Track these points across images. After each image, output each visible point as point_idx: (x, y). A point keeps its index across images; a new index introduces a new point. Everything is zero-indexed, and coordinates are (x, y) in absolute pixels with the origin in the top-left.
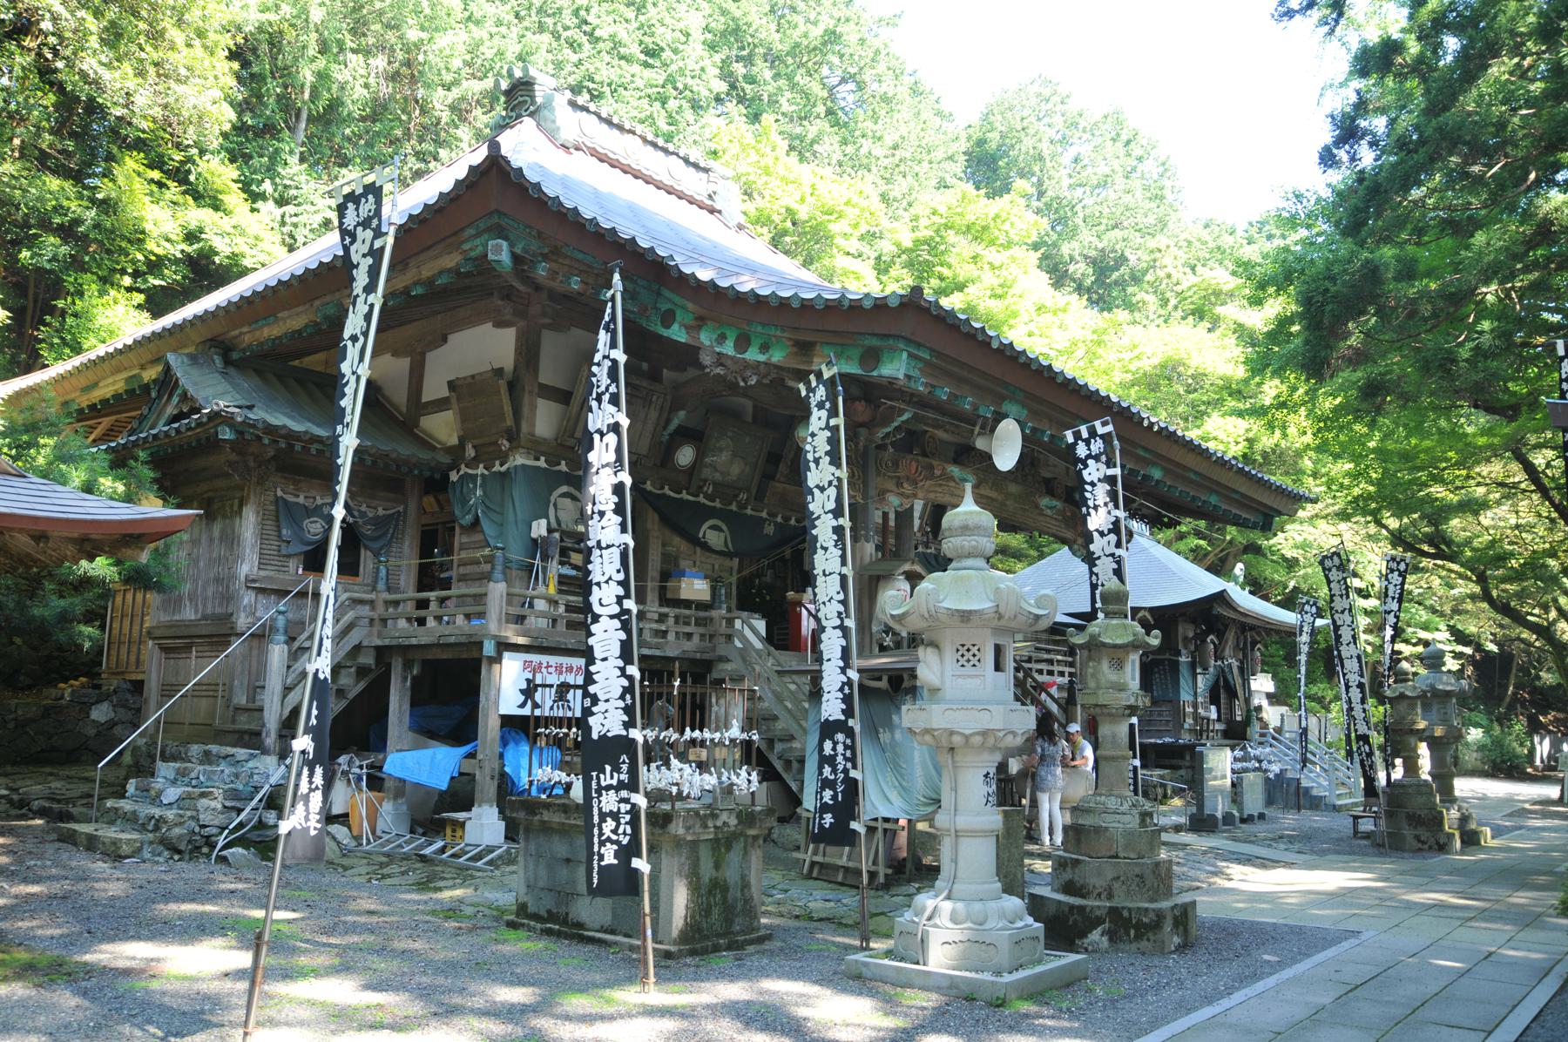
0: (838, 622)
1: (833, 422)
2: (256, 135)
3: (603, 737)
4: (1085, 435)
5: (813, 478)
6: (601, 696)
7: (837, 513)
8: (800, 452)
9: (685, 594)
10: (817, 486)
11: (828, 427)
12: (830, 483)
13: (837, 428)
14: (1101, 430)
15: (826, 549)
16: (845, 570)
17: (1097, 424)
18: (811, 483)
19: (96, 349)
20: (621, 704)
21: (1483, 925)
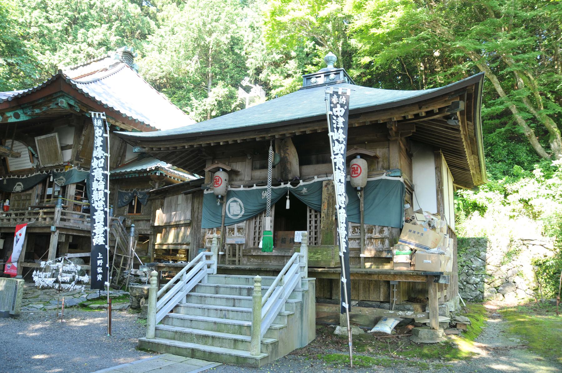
0: (102, 208)
1: (105, 135)
2: (434, 355)
3: (97, 245)
4: (97, 116)
5: (95, 154)
6: (97, 233)
7: (104, 168)
8: (93, 143)
9: (17, 190)
10: (95, 157)
11: (102, 136)
12: (102, 157)
13: (107, 138)
14: (102, 117)
15: (99, 181)
16: (106, 191)
17: (101, 114)
18: (94, 155)
19: (13, 112)
20: (103, 235)
21: (472, 113)
